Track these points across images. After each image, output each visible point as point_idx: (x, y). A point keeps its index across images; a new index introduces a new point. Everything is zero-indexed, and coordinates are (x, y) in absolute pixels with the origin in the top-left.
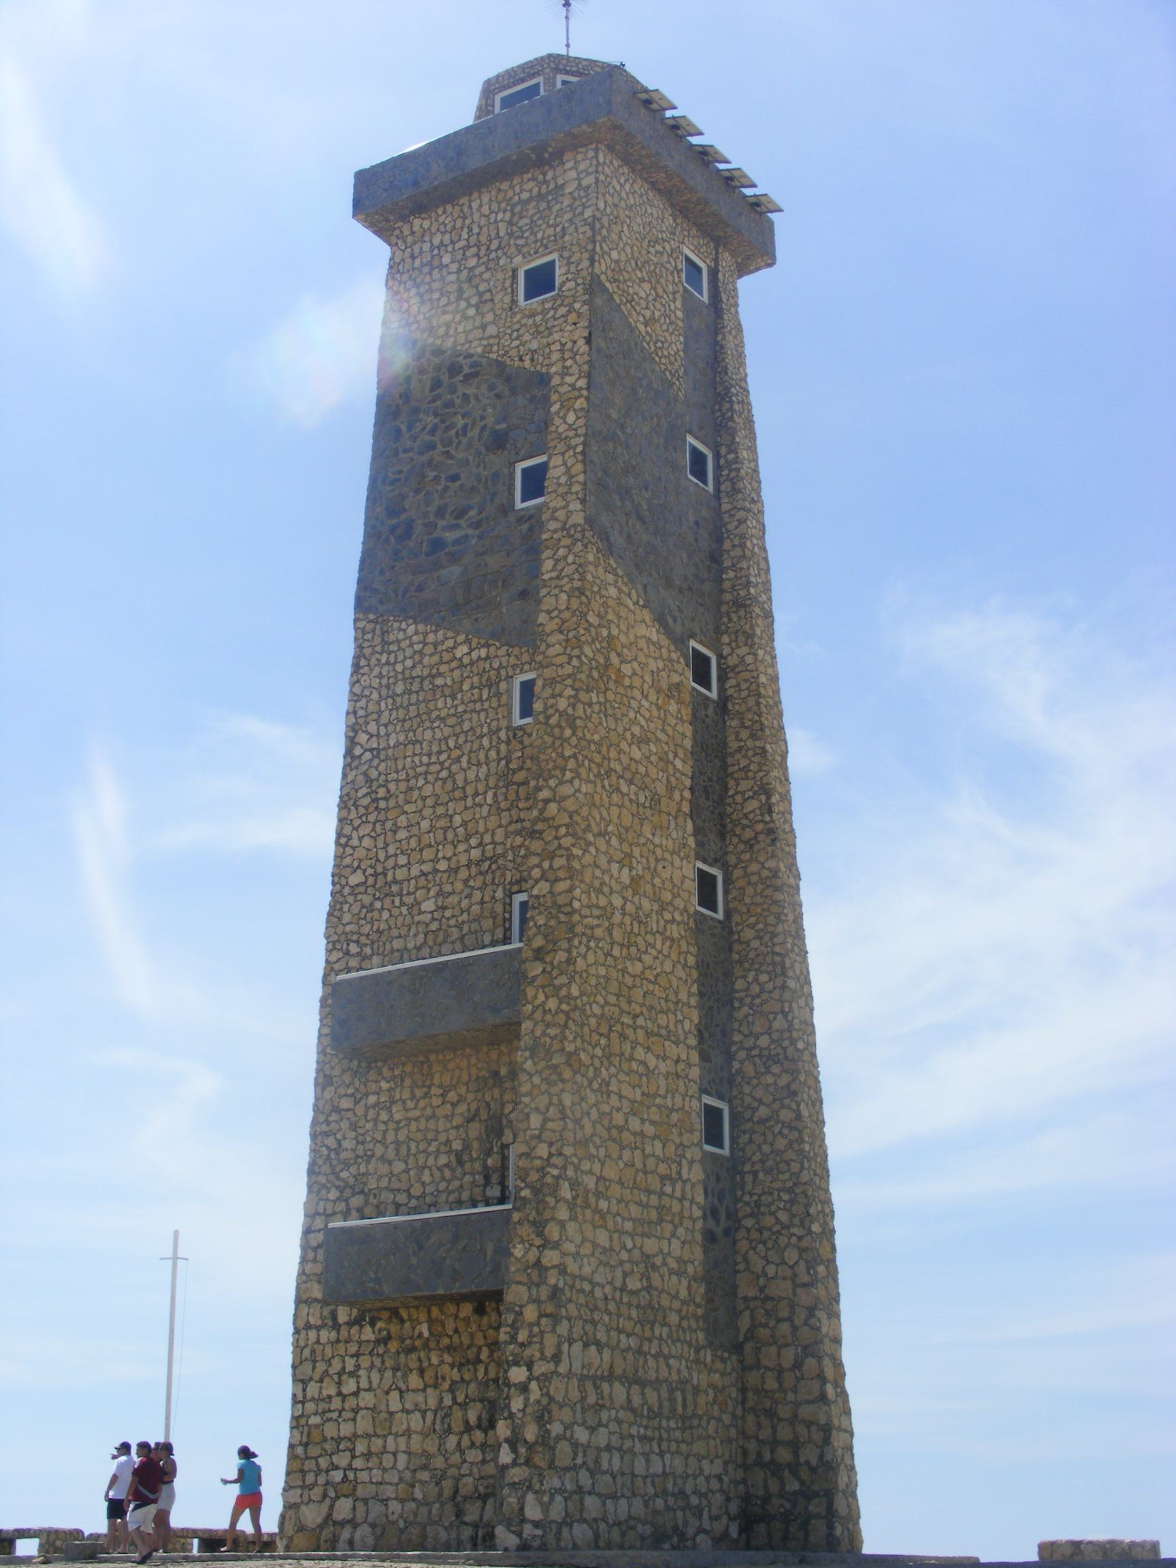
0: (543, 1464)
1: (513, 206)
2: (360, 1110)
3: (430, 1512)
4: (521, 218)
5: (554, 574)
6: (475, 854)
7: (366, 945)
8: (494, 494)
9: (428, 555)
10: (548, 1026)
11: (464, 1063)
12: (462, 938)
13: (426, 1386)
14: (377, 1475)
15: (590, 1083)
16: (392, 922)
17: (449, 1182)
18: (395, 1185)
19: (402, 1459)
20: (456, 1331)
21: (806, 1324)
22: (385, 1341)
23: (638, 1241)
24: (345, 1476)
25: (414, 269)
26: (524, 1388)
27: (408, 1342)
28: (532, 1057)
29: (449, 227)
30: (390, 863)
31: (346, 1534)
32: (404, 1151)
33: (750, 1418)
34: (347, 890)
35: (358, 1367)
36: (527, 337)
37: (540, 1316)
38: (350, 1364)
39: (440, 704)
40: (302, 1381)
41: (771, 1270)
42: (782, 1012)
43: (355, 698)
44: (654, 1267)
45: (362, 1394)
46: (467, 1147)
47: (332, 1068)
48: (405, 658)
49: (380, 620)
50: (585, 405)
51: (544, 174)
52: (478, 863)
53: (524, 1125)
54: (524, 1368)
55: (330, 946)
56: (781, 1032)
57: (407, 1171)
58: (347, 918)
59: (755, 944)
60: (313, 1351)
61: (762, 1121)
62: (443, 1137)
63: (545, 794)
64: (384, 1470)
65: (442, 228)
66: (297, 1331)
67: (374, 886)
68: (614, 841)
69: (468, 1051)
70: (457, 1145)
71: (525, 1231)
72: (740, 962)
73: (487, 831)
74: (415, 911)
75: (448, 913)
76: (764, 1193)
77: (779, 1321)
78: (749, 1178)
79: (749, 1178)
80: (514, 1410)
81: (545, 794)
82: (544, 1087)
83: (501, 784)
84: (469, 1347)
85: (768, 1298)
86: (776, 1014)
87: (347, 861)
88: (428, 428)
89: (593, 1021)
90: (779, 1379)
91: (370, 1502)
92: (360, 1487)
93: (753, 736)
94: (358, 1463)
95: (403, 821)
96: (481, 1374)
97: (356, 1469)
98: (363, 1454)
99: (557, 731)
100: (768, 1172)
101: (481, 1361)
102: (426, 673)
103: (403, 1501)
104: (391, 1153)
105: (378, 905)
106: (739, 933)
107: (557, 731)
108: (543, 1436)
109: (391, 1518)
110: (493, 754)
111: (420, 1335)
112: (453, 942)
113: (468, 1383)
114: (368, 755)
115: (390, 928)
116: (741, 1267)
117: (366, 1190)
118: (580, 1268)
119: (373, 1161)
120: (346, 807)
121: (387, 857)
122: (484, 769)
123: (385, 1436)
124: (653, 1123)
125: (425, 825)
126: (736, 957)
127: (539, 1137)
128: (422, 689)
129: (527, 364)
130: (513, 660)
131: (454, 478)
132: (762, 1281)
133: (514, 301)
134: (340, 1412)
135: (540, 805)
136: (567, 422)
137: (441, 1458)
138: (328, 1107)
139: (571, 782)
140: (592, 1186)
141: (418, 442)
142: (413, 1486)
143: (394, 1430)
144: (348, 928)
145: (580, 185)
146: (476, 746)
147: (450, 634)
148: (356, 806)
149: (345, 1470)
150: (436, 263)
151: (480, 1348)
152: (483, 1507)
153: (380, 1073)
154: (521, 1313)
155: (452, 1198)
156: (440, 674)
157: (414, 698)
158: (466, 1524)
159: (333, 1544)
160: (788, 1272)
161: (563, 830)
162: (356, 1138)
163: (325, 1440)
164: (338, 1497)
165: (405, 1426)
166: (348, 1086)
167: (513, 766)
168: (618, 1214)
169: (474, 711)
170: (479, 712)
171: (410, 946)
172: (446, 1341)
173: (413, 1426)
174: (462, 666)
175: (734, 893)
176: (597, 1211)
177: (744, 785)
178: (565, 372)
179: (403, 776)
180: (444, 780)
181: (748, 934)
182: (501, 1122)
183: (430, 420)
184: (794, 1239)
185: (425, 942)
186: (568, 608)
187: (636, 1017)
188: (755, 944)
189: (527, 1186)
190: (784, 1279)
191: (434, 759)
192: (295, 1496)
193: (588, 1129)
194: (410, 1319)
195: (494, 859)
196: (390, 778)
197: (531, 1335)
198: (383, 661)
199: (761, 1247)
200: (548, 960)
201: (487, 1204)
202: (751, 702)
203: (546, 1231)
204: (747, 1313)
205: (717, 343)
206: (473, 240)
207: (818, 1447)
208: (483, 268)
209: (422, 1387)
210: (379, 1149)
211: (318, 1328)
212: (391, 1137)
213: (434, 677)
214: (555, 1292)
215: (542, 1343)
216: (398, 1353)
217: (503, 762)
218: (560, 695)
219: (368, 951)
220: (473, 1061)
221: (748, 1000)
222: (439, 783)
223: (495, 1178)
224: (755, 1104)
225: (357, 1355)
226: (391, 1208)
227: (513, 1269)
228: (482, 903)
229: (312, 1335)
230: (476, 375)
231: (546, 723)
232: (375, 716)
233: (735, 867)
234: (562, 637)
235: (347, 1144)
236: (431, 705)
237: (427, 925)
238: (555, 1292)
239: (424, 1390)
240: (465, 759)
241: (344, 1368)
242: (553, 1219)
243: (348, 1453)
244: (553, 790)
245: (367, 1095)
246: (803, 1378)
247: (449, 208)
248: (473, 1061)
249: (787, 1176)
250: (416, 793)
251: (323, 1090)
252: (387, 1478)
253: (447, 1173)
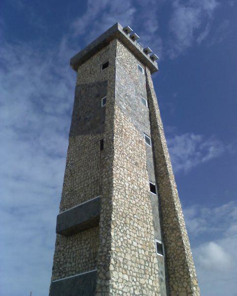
6: (93, 180)
15: (120, 230)
18: (73, 269)
23: (138, 279)
32: (75, 259)
41: (180, 289)
44: (144, 288)
57: (75, 265)
58: (64, 202)
59: (166, 201)
62: (84, 254)
68: (125, 170)
72: (163, 206)
78: (171, 263)
79: (171, 263)
89: (120, 213)
104: (72, 261)
116: (171, 289)
118: (118, 286)
124: (141, 245)
125: (82, 177)
140: (121, 261)
168: (131, 270)
175: (160, 190)
176: (123, 268)
187: (134, 215)
188: (166, 201)
190: (184, 291)
193: (120, 244)
199: (176, 283)
210: (69, 260)
212: (72, 256)
228: (94, 191)
244: (108, 157)
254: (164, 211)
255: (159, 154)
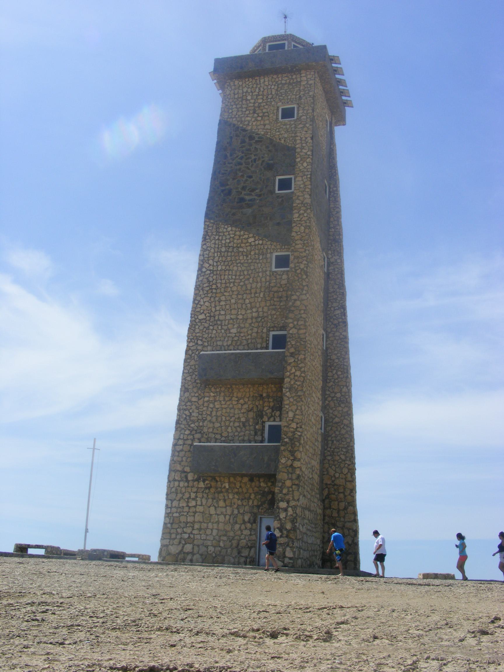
0: (293, 538)
1: (278, 85)
2: (201, 402)
3: (227, 551)
4: (281, 89)
5: (299, 219)
6: (255, 315)
7: (205, 342)
8: (267, 186)
9: (238, 203)
10: (296, 381)
11: (248, 390)
12: (248, 344)
13: (226, 506)
14: (203, 536)
16: (217, 335)
17: (239, 433)
19: (215, 532)
20: (241, 487)
21: (350, 495)
22: (209, 488)
24: (189, 536)
25: (235, 98)
26: (286, 510)
27: (219, 489)
28: (289, 391)
29: (250, 86)
30: (217, 313)
31: (189, 557)
32: (219, 419)
33: (326, 526)
34: (197, 320)
35: (196, 497)
36: (283, 132)
37: (293, 485)
38: (193, 495)
39: (241, 258)
40: (171, 500)
41: (337, 475)
42: (346, 386)
43: (203, 250)
45: (198, 507)
46: (247, 420)
47: (189, 386)
48: (226, 239)
49: (216, 223)
50: (311, 161)
51: (292, 76)
52: (256, 318)
53: (286, 415)
54: (286, 503)
55: (189, 340)
56: (345, 393)
58: (197, 331)
60: (176, 489)
61: (336, 423)
62: (237, 416)
63: (294, 297)
64: (207, 535)
65: (247, 86)
66: (169, 481)
67: (209, 320)
69: (249, 386)
70: (243, 419)
71: (286, 453)
72: (330, 366)
73: (260, 307)
74: (228, 332)
75: (242, 335)
76: (336, 448)
77: (339, 493)
78: (330, 442)
79: (330, 442)
80: (281, 517)
81: (294, 297)
82: (295, 403)
83: (267, 291)
84: (246, 493)
85: (335, 485)
86: (344, 386)
87: (198, 310)
88: (239, 157)
90: (338, 512)
91: (200, 547)
92: (195, 540)
93: (339, 288)
94: (195, 532)
95: (223, 298)
96: (251, 503)
97: (194, 534)
98: (197, 529)
99: (300, 275)
100: (338, 441)
101: (251, 499)
102: (235, 245)
103: (215, 547)
104: (214, 419)
105: (211, 328)
106: (330, 356)
107: (300, 275)
108: (294, 528)
109: (209, 552)
110: (263, 279)
111: (225, 487)
112: (244, 346)
113: (245, 506)
114: (208, 272)
115: (216, 337)
117: (202, 432)
119: (206, 422)
120: (198, 290)
121: (216, 311)
122: (259, 284)
123: (208, 523)
125: (233, 301)
126: (329, 364)
127: (292, 420)
128: (233, 251)
129: (282, 142)
130: (273, 247)
131: (250, 177)
132: (333, 479)
133: (277, 119)
134: (188, 513)
135: (293, 301)
136: (303, 166)
137: (232, 532)
138: (186, 400)
139: (306, 294)
141: (234, 161)
142: (219, 542)
143: (212, 521)
144: (198, 335)
145: (307, 83)
146: (256, 276)
147: (246, 233)
148: (203, 290)
149: (189, 534)
150: (244, 98)
151: (251, 494)
152: (250, 551)
153: (210, 390)
154: (284, 483)
155: (240, 439)
156: (241, 247)
157: (229, 254)
158: (242, 556)
159: (184, 560)
160: (344, 476)
161: (302, 312)
162: (198, 413)
163: (180, 522)
164: (186, 544)
165: (217, 520)
166: (195, 393)
167: (272, 285)
169: (256, 262)
170: (258, 263)
171: (225, 344)
172: (236, 490)
173: (220, 520)
174: (251, 245)
175: (329, 342)
177: (335, 305)
178: (302, 148)
179: (224, 281)
180: (242, 286)
181: (334, 357)
182: (262, 414)
183: (240, 154)
184: (346, 465)
185: (232, 344)
186: (304, 232)
189: (287, 438)
190: (342, 478)
191: (237, 277)
192: (166, 542)
194: (220, 481)
195: (263, 317)
196: (218, 281)
197: (289, 491)
198: (217, 238)
199: (333, 467)
200: (296, 357)
201: (256, 443)
202: (339, 276)
203: (295, 454)
204: (327, 489)
205: (331, 148)
206: (261, 93)
207: (352, 537)
208: (265, 104)
209: (224, 506)
210: (209, 418)
211: (179, 481)
212: (214, 413)
213: (238, 247)
214: (298, 477)
215: (293, 494)
216: (215, 493)
217: (268, 283)
218: (301, 263)
219: (206, 344)
220: (251, 389)
221: (333, 380)
222: (240, 287)
223: (259, 433)
224: (334, 417)
225: (196, 492)
226: (213, 440)
227: (280, 467)
228: (257, 333)
229: (176, 483)
230: (261, 141)
231: (296, 272)
232: (212, 258)
233: (330, 333)
234: (302, 242)
235: (194, 414)
236: (237, 258)
237: (233, 338)
238: (298, 477)
239: (226, 507)
240: (251, 279)
241: (190, 497)
242: (298, 450)
243: (191, 528)
244: (298, 297)
245: (204, 397)
246: (347, 513)
247: (251, 80)
248: (251, 389)
249: (345, 443)
250: (229, 289)
251: (184, 393)
252: (208, 538)
253: (239, 429)
254: (330, 374)
255: (336, 287)
